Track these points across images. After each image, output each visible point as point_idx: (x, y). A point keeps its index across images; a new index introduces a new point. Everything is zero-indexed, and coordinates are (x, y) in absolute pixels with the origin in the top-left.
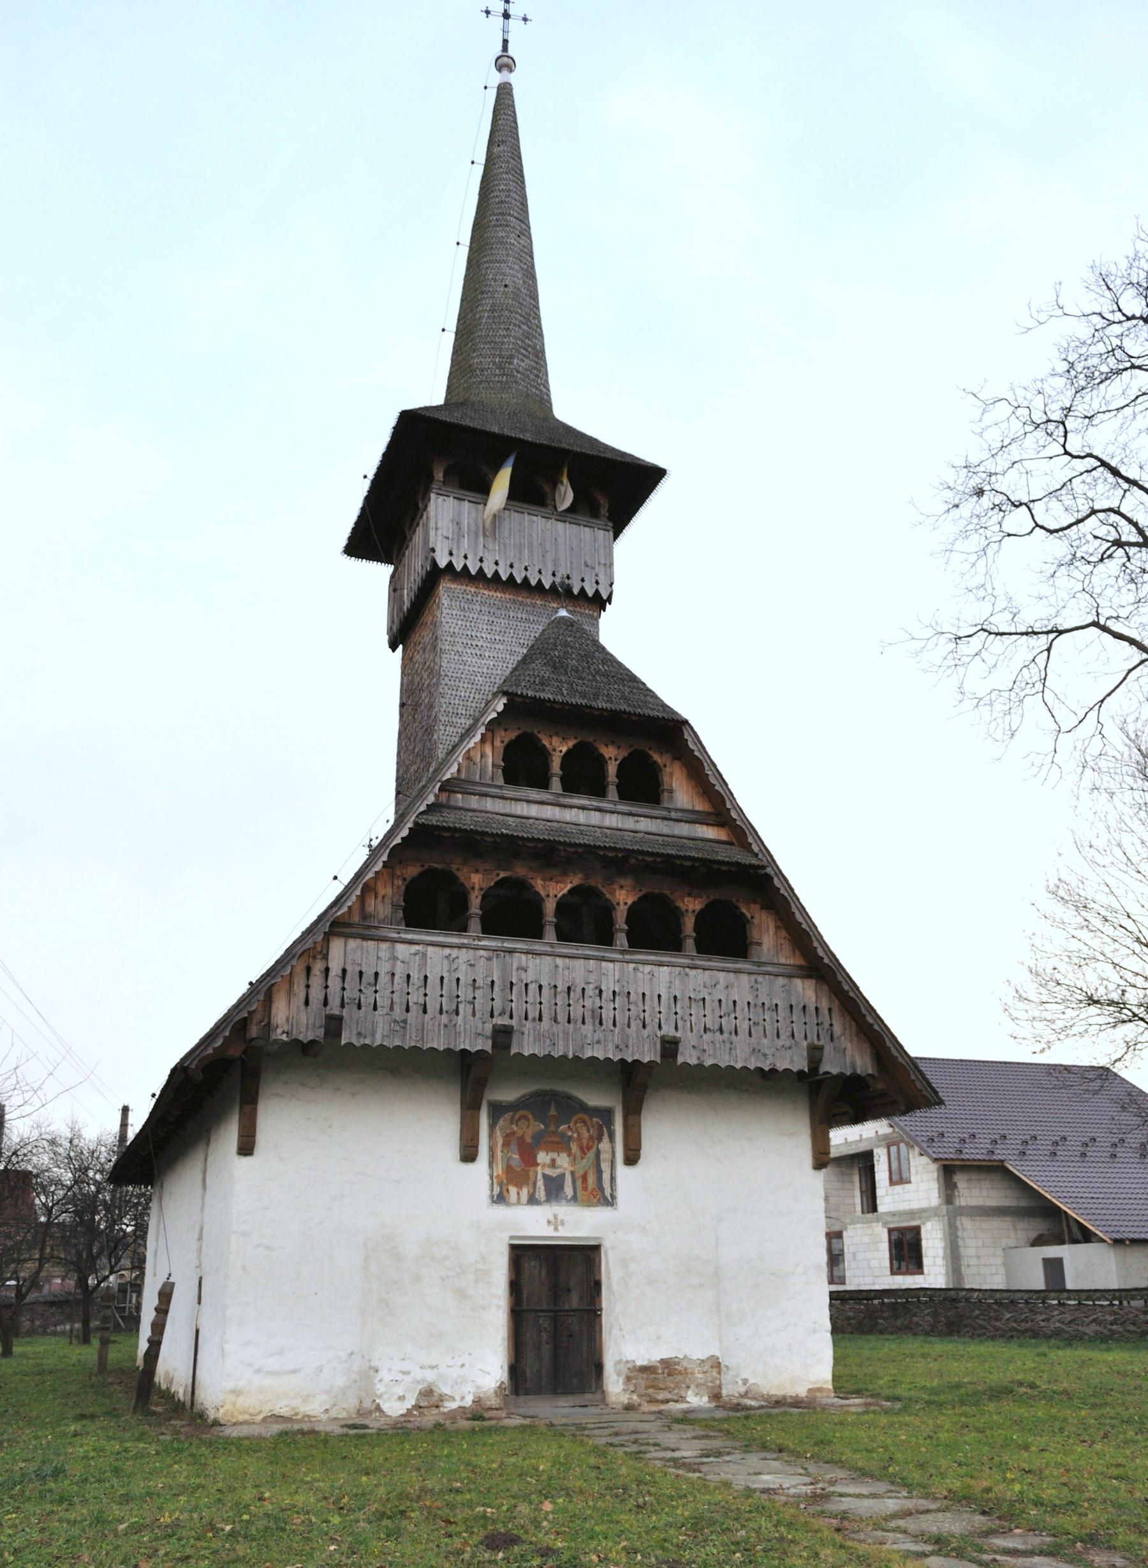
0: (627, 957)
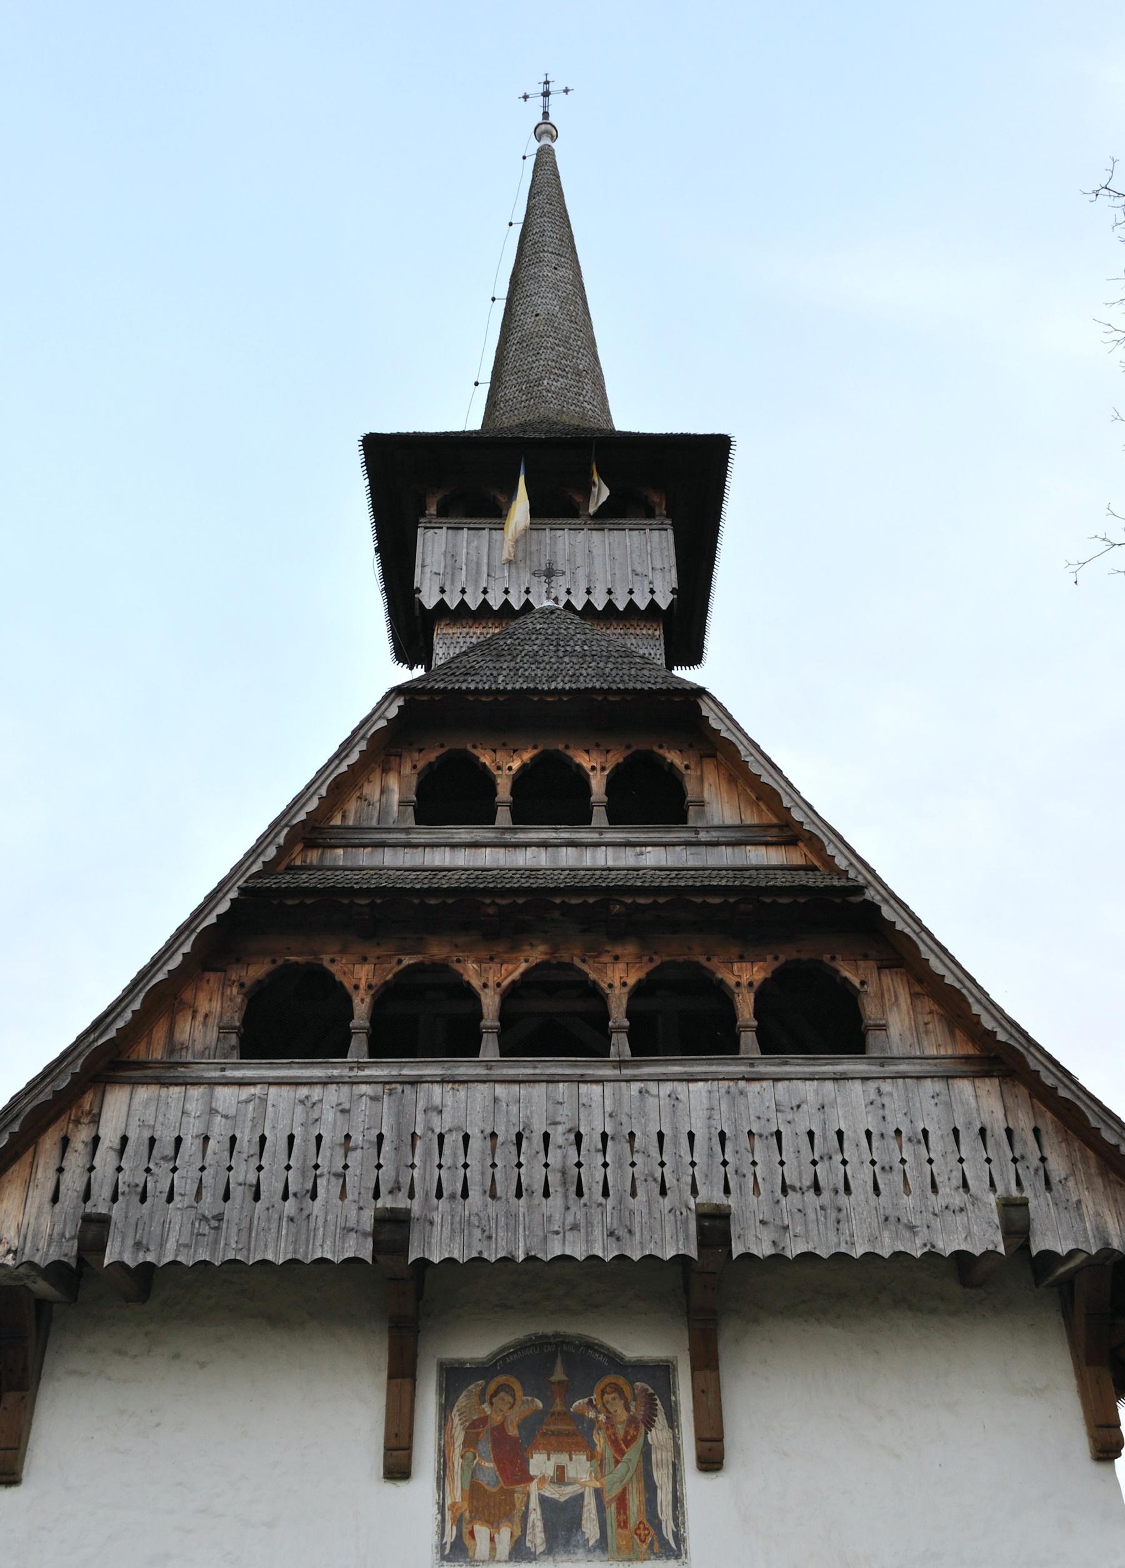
0: (628, 1072)
